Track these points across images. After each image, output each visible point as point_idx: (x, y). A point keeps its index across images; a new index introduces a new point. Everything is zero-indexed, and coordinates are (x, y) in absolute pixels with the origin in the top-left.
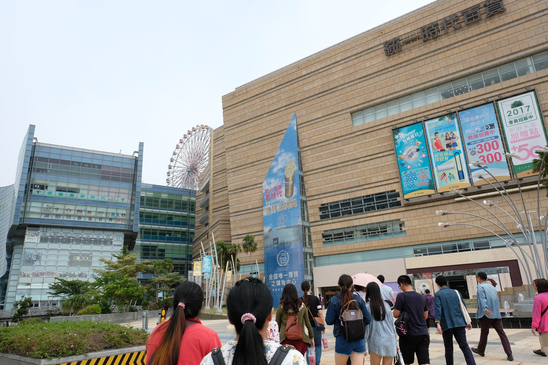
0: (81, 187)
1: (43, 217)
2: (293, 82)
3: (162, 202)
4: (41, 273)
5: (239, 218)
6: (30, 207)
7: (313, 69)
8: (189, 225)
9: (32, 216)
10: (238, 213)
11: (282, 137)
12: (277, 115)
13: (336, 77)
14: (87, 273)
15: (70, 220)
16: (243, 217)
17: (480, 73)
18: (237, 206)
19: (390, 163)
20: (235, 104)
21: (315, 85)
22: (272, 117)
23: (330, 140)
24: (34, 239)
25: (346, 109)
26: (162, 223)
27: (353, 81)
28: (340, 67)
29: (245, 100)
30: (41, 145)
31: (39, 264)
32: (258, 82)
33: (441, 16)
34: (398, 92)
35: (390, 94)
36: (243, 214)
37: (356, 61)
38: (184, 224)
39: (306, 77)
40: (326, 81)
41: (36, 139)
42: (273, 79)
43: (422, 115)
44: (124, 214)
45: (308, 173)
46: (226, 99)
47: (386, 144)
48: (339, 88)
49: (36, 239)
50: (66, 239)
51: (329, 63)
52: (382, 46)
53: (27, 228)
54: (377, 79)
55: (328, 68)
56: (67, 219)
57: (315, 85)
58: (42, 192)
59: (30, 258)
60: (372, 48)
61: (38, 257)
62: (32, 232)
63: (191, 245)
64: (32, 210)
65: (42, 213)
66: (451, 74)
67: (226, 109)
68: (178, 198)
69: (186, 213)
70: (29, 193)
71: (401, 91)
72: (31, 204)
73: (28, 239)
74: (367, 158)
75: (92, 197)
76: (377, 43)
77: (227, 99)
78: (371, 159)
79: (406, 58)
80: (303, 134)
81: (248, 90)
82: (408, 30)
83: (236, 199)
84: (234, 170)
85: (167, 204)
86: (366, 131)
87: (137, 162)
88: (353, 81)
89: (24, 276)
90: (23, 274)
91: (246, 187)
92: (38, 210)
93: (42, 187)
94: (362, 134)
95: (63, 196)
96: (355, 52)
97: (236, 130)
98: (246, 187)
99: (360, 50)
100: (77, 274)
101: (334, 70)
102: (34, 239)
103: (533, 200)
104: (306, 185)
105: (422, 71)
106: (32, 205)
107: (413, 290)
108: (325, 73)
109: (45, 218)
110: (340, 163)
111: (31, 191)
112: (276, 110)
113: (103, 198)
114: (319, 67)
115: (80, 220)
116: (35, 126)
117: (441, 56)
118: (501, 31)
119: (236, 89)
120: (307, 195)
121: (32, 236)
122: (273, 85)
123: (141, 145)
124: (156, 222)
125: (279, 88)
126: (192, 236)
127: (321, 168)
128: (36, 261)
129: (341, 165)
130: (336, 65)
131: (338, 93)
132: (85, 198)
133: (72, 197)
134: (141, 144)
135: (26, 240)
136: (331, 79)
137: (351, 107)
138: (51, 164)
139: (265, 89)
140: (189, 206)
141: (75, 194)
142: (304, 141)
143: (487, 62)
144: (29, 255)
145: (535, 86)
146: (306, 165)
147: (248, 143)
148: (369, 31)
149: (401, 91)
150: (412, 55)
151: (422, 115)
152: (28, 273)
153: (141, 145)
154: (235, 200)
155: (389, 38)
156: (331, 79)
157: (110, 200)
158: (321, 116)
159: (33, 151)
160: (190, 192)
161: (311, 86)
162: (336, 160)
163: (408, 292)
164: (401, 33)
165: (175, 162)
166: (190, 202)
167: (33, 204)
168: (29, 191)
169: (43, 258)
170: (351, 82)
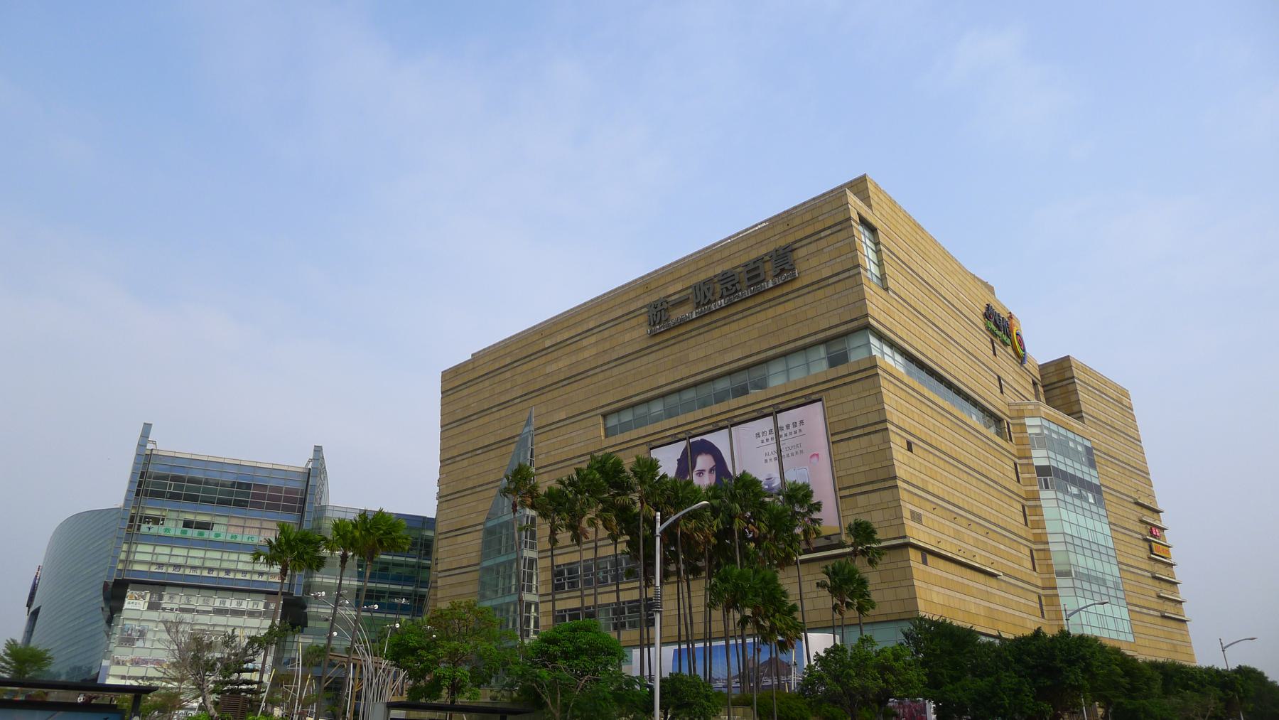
0: (217, 520)
1: (153, 569)
2: (533, 357)
4: (144, 660)
6: (135, 552)
7: (559, 339)
8: (417, 581)
9: (137, 567)
11: (513, 446)
12: (508, 411)
13: (586, 354)
15: (195, 574)
17: (843, 338)
18: (448, 559)
20: (458, 386)
21: (561, 364)
22: (503, 413)
24: (139, 604)
25: (597, 409)
27: (608, 363)
28: (593, 339)
29: (471, 381)
30: (160, 453)
31: (142, 646)
32: (802, 212)
33: (719, 270)
34: (662, 386)
37: (613, 330)
38: (408, 580)
39: (550, 350)
40: (574, 359)
41: (154, 442)
43: (770, 403)
46: (444, 374)
48: (589, 373)
49: (142, 605)
51: (580, 331)
53: (130, 586)
54: (637, 363)
55: (578, 338)
56: (191, 573)
57: (561, 364)
58: (155, 530)
59: (130, 635)
60: (633, 311)
61: (142, 634)
62: (136, 593)
64: (138, 557)
65: (152, 563)
66: (727, 364)
69: (414, 560)
70: (136, 530)
71: (665, 385)
72: (136, 549)
73: (129, 603)
75: (232, 537)
76: (640, 304)
81: (476, 364)
82: (679, 287)
84: (449, 498)
88: (608, 363)
89: (118, 663)
90: (116, 660)
91: (463, 528)
92: (148, 558)
93: (156, 521)
95: (187, 535)
96: (613, 316)
98: (463, 528)
99: (619, 313)
101: (585, 343)
102: (139, 604)
103: (791, 580)
105: (692, 357)
106: (138, 550)
108: (573, 347)
109: (157, 570)
111: (139, 526)
112: (508, 401)
113: (250, 539)
114: (566, 336)
115: (211, 575)
116: (151, 425)
118: (788, 300)
119: (472, 355)
121: (136, 599)
122: (508, 361)
123: (318, 450)
125: (515, 365)
128: (138, 640)
130: (588, 334)
131: (587, 381)
132: (222, 538)
133: (201, 537)
134: (318, 449)
135: (126, 606)
136: (581, 356)
137: (603, 406)
139: (497, 366)
141: (206, 532)
143: (770, 349)
144: (128, 630)
145: (820, 395)
147: (470, 455)
148: (804, 203)
149: (665, 385)
151: (770, 403)
152: (124, 658)
153: (318, 450)
154: (446, 549)
155: (654, 297)
156: (581, 356)
157: (261, 541)
158: (837, 322)
159: (146, 464)
161: (554, 367)
163: (49, 702)
164: (671, 290)
166: (422, 539)
167: (141, 548)
168: (136, 527)
169: (149, 635)
170: (605, 364)
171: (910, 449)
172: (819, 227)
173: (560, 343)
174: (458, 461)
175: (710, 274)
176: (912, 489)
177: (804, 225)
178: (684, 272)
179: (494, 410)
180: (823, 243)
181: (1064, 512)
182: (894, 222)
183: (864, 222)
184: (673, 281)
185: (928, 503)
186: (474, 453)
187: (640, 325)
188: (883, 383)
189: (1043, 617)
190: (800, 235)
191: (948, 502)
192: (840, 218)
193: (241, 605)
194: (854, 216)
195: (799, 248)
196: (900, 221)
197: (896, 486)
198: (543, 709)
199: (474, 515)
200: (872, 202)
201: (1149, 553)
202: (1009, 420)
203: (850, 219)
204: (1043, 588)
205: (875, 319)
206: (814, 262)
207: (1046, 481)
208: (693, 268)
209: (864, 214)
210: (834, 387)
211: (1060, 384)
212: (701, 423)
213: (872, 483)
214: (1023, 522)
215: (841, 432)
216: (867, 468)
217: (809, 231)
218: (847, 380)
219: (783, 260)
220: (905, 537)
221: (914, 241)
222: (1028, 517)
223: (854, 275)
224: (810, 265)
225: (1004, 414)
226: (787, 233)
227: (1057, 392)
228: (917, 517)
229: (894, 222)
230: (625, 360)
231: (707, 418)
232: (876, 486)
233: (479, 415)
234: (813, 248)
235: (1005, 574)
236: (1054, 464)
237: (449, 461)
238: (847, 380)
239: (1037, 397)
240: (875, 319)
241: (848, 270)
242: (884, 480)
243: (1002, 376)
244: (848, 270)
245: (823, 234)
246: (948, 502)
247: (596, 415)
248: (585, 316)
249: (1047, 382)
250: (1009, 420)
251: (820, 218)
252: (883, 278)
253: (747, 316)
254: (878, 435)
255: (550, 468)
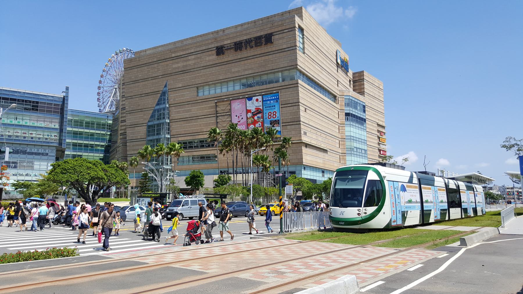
3: (86, 123)
5: (132, 143)
7: (178, 54)
10: (132, 140)
13: (190, 62)
14: (31, 174)
16: (134, 143)
19: (213, 121)
21: (179, 65)
23: (185, 102)
26: (87, 139)
27: (199, 67)
28: (193, 57)
33: (245, 38)
35: (217, 80)
36: (204, 102)
39: (174, 58)
40: (185, 64)
42: (155, 55)
44: (56, 136)
45: (172, 121)
47: (212, 110)
50: (15, 151)
52: (215, 49)
57: (179, 65)
63: (108, 155)
67: (126, 69)
68: (98, 121)
74: (202, 117)
76: (213, 46)
77: (127, 62)
78: (205, 118)
79: (226, 60)
80: (171, 96)
81: (140, 59)
82: (229, 42)
83: (131, 131)
85: (89, 125)
86: (203, 100)
87: (64, 100)
88: (199, 67)
94: (201, 102)
96: (201, 49)
97: (132, 85)
99: (204, 48)
100: (24, 174)
101: (190, 57)
104: (171, 128)
105: (233, 70)
107: (3, 198)
110: (189, 117)
114: (181, 53)
117: (242, 63)
120: (171, 134)
123: (67, 88)
124: (81, 138)
125: (159, 62)
126: (109, 148)
127: (180, 119)
129: (190, 119)
130: (191, 54)
136: (188, 63)
138: (3, 101)
140: (107, 126)
142: (171, 100)
143: (262, 72)
145: (278, 91)
146: (172, 116)
150: (230, 59)
153: (67, 88)
154: (130, 131)
155: (219, 44)
156: (188, 63)
160: (108, 117)
162: (187, 115)
164: (226, 42)
165: (104, 78)
171: (305, 111)
172: (284, 28)
173: (179, 56)
174: (134, 98)
175: (241, 39)
176: (305, 124)
177: (278, 26)
178: (231, 36)
179: (150, 79)
180: (284, 35)
181: (352, 128)
182: (310, 25)
183: (300, 27)
184: (227, 39)
185: (309, 128)
186: (141, 96)
187: (213, 55)
188: (300, 89)
189: (340, 162)
190: (276, 30)
191: (315, 127)
192: (292, 26)
193: (39, 151)
194: (297, 26)
195: (276, 35)
196: (312, 23)
197: (300, 124)
198: (202, 185)
199: (143, 120)
200: (304, 18)
201: (378, 141)
202: (339, 96)
203: (295, 27)
204: (342, 153)
205: (300, 66)
206: (281, 41)
207: (348, 118)
208: (235, 35)
209: (300, 24)
210: (283, 89)
211: (359, 81)
212: (235, 95)
213: (292, 122)
214: (338, 132)
215: (284, 104)
216: (291, 117)
217: (280, 29)
218: (284, 87)
219: (268, 39)
220: (301, 140)
221: (316, 31)
222: (340, 130)
223: (294, 49)
224: (279, 42)
225: (337, 94)
226: (271, 28)
227: (357, 84)
228: (305, 133)
229: (310, 25)
230: (206, 67)
231: (238, 94)
232: (294, 123)
233: (143, 80)
234: (281, 36)
235: (330, 150)
236: (351, 112)
237: (130, 98)
238: (288, 87)
239: (350, 86)
240: (300, 66)
241: (292, 47)
242: (297, 122)
243: (339, 80)
244: (292, 47)
245: (285, 31)
246: (315, 127)
247: (194, 87)
248: (190, 47)
249: (355, 79)
250: (339, 96)
251: (284, 25)
252: (304, 49)
253: (254, 58)
254: (296, 107)
255: (175, 105)
